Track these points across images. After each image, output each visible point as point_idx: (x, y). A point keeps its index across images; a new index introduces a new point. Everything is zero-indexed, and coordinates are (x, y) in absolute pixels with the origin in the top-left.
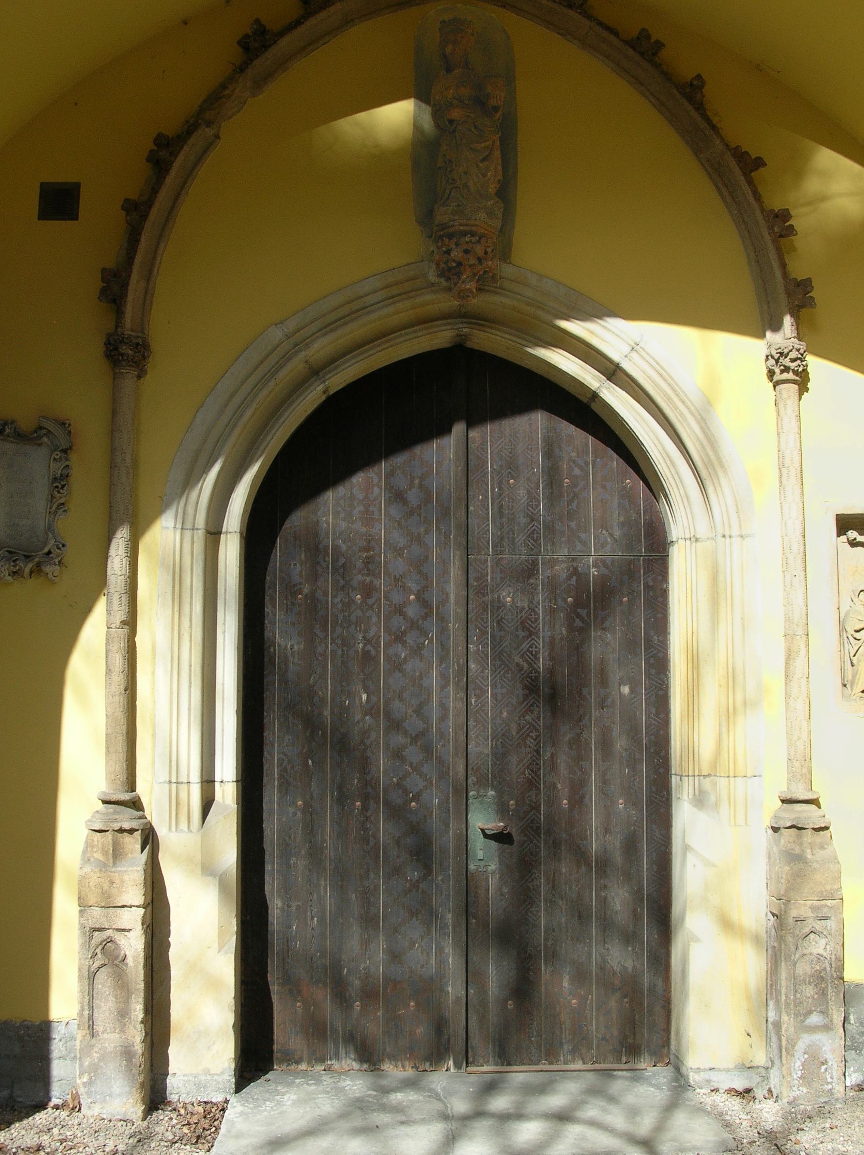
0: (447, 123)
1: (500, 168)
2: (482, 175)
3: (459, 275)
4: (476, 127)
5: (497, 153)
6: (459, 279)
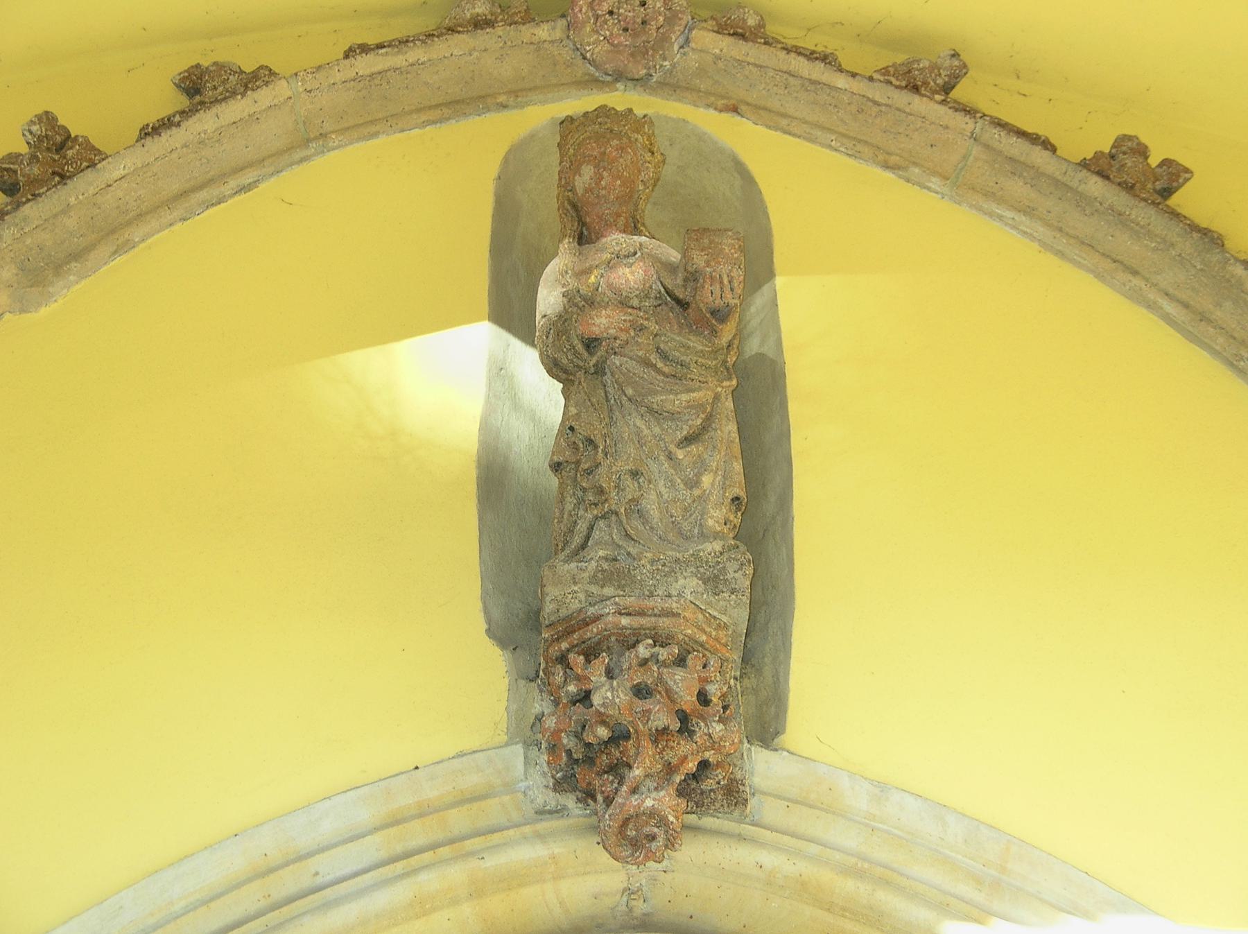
0: (580, 347)
1: (738, 467)
2: (685, 484)
3: (618, 769)
4: (664, 356)
5: (729, 429)
6: (621, 783)
